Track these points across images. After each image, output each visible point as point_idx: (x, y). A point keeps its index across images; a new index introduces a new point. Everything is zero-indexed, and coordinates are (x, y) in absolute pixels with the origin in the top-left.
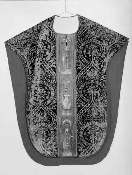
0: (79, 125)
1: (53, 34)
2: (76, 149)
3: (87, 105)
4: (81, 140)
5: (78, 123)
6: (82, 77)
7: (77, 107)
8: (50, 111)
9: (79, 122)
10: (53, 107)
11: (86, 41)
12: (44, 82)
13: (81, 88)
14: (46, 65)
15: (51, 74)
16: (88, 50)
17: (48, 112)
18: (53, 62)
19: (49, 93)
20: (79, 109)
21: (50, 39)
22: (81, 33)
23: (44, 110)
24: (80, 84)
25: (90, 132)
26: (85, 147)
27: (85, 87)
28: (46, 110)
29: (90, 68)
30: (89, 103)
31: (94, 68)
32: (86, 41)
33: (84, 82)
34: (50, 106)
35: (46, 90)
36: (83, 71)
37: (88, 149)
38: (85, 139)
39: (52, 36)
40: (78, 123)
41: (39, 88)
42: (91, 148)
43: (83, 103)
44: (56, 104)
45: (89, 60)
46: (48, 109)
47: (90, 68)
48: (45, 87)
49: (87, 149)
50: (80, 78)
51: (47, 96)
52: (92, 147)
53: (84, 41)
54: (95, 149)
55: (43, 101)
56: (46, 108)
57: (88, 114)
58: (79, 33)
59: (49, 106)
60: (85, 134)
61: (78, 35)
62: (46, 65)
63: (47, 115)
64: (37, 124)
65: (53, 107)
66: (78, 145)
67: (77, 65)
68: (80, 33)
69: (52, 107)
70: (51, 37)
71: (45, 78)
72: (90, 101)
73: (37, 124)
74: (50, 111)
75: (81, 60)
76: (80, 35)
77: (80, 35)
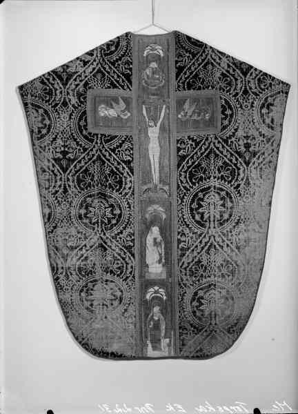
0: (182, 187)
2: (175, 244)
3: (201, 149)
4: (185, 222)
7: (176, 68)
8: (118, 76)
9: (182, 182)
10: (127, 241)
11: (199, 281)
13: (188, 199)
14: (110, 68)
16: (202, 301)
21: (121, 193)
22: (189, 167)
24: (185, 187)
27: (196, 195)
28: (108, 73)
29: (207, 152)
30: (204, 144)
32: (199, 281)
33: (194, 184)
37: (201, 242)
38: (194, 218)
41: (96, 201)
43: (188, 57)
44: (132, 149)
45: (203, 225)
47: (207, 152)
49: (199, 241)
51: (115, 300)
53: (194, 184)
54: (215, 241)
55: (105, 140)
56: (110, 155)
57: (200, 79)
58: (181, 78)
59: (118, 239)
61: (179, 82)
62: (110, 68)
65: (126, 69)
66: (180, 328)
67: (181, 331)
68: (186, 168)
71: (108, 181)
74: (118, 75)
75: (184, 48)
77: (185, 172)
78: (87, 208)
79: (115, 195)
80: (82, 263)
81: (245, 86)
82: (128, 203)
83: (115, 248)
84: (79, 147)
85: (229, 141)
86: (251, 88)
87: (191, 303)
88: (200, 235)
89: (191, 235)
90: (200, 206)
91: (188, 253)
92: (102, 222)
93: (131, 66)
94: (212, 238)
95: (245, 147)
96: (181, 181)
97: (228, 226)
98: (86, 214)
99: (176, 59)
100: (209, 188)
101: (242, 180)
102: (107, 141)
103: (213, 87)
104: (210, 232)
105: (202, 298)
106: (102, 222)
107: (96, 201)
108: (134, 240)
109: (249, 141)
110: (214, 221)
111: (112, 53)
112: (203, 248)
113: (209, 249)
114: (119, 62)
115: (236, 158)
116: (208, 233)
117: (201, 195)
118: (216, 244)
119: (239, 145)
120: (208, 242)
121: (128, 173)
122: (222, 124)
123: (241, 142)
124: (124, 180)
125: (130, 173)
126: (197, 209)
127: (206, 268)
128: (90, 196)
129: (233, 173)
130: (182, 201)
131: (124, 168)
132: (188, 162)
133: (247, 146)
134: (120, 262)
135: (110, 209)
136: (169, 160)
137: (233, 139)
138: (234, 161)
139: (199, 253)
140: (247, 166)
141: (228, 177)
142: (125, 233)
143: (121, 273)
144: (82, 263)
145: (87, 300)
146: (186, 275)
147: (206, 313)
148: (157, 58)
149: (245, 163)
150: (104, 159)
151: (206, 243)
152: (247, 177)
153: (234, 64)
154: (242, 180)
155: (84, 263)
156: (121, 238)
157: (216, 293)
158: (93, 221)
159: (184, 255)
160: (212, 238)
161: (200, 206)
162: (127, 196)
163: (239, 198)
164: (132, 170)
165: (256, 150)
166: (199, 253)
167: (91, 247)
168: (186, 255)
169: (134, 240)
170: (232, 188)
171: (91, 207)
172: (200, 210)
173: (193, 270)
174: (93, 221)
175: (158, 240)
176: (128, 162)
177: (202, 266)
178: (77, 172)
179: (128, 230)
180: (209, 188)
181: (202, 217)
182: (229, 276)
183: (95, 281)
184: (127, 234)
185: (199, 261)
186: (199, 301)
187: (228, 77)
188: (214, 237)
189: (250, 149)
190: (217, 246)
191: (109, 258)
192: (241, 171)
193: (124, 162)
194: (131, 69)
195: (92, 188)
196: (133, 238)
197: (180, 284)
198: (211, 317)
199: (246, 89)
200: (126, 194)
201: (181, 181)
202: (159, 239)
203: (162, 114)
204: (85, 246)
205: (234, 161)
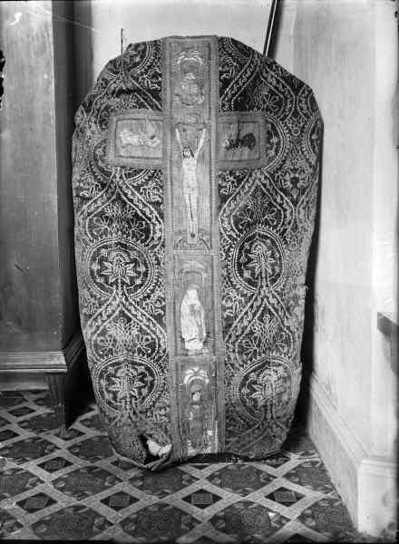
0: (226, 237)
4: (232, 282)
5: (222, 231)
7: (220, 80)
10: (156, 308)
11: (251, 360)
12: (136, 354)
15: (152, 331)
19: (150, 378)
20: (225, 83)
23: (127, 201)
24: (230, 236)
25: (261, 384)
26: (235, 180)
28: (136, 316)
30: (249, 66)
31: (270, 312)
32: (251, 360)
34: (147, 304)
35: (135, 261)
36: (237, 82)
37: (252, 307)
40: (222, 231)
41: (114, 254)
44: (161, 187)
45: (254, 285)
48: (131, 253)
51: (144, 387)
52: (262, 300)
56: (133, 194)
59: (141, 191)
60: (247, 274)
61: (224, 99)
62: (136, 309)
63: (141, 330)
64: (112, 354)
65: (152, 83)
72: (252, 62)
73: (112, 354)
76: (233, 343)
77: (233, 343)
78: (100, 263)
79: (140, 246)
80: (99, 339)
81: (296, 107)
82: (157, 259)
83: (140, 316)
84: (96, 183)
85: (276, 175)
86: (301, 109)
87: (240, 390)
88: (251, 298)
89: (239, 297)
90: (250, 260)
91: (235, 323)
92: (123, 283)
93: (160, 79)
94: (265, 300)
95: (292, 182)
96: (224, 228)
97: (281, 281)
98: (99, 272)
99: (221, 69)
100: (254, 236)
101: (289, 223)
102: (129, 176)
103: (259, 109)
104: (262, 292)
105: (255, 383)
106: (123, 283)
107: (114, 254)
108: (164, 307)
109: (297, 175)
110: (266, 278)
111: (136, 65)
112: (254, 315)
113: (262, 315)
114: (145, 76)
115: (281, 196)
116: (260, 293)
117: (247, 246)
118: (270, 307)
119: (285, 181)
120: (260, 306)
121: (157, 219)
122: (267, 155)
123: (287, 177)
124: (152, 228)
125: (160, 219)
126: (245, 264)
127: (260, 341)
128: (105, 247)
129: (278, 216)
130: (228, 256)
131: (151, 212)
132: (229, 205)
133: (294, 181)
134: (150, 338)
135: (132, 265)
136: (211, 200)
137: (280, 173)
138: (279, 200)
139: (250, 322)
140: (295, 206)
141: (273, 221)
142: (154, 297)
143: (153, 351)
144: (99, 339)
145: (109, 392)
146: (234, 351)
147: (261, 404)
148: (193, 68)
149: (293, 203)
150: (124, 198)
151: (259, 307)
152: (295, 219)
153: (283, 78)
154: (289, 223)
155: (101, 338)
156: (147, 304)
157: (272, 373)
158: (111, 281)
159: (230, 325)
160: (265, 300)
161: (250, 260)
162: (156, 250)
163: (284, 246)
164: (162, 215)
165: (305, 186)
166: (250, 322)
167: (109, 317)
168: (233, 326)
169: (164, 307)
170: (278, 235)
171: (107, 261)
172: (250, 265)
173: (244, 345)
174: (111, 281)
175: (196, 308)
176: (158, 204)
177: (256, 338)
178: (233, 95)
179: (158, 293)
180: (254, 236)
181: (253, 275)
182: (283, 347)
183: (118, 364)
184: (155, 298)
185: (252, 333)
186: (250, 386)
187: (277, 95)
188: (268, 298)
189: (298, 185)
190: (272, 310)
191: (135, 332)
192: (288, 213)
193: (151, 203)
194: (159, 83)
195: (109, 236)
196: (163, 303)
197: (226, 364)
198: (266, 410)
199: (296, 110)
200: (154, 246)
201: (224, 228)
202: (198, 304)
203: (202, 141)
204: (101, 314)
205: (279, 200)
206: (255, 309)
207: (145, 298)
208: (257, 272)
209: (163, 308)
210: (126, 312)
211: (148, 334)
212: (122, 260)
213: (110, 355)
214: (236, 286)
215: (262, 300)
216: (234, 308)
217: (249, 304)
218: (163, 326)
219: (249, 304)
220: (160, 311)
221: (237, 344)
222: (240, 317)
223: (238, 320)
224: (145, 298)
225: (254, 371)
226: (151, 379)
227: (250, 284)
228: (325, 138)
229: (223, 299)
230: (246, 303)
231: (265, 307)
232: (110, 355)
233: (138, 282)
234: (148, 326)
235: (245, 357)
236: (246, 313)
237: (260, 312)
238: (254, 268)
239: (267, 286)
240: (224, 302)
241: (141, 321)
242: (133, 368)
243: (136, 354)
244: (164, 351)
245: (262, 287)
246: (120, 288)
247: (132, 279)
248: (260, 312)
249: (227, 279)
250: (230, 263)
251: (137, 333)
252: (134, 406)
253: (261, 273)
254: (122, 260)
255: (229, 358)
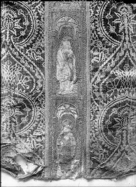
1: (37, 84)
4: (99, 35)
6: (103, 82)
10: (37, 143)
11: (113, 97)
12: (17, 89)
17: (23, 64)
18: (35, 50)
19: (26, 23)
31: (130, 63)
35: (21, 17)
39: (35, 89)
42: (119, 153)
46: (25, 59)
50: (98, 84)
51: (24, 116)
52: (125, 52)
59: (27, 52)
69: (33, 54)
70: (32, 90)
82: (38, 14)
88: (115, 49)
94: (127, 52)
113: (124, 64)
118: (130, 59)
130: (95, 12)
134: (29, 78)
135: (19, 20)
146: (99, 91)
151: (121, 58)
156: (30, 52)
160: (127, 52)
161: (115, 17)
162: (37, 7)
172: (116, 22)
179: (38, 43)
181: (117, 29)
184: (36, 47)
188: (129, 52)
197: (92, 101)
198: (122, 137)
206: (117, 59)
207: (28, 47)
208: (121, 29)
209: (43, 55)
210: (12, 57)
211: (27, 74)
212: (11, 16)
213: (115, 97)
214: (102, 38)
215: (125, 52)
216: (100, 56)
217: (113, 55)
218: (42, 69)
219: (113, 55)
220: (40, 57)
221: (101, 85)
222: (105, 63)
223: (103, 65)
224: (28, 47)
225: (115, 106)
226: (29, 110)
227: (113, 38)
228: (100, 180)
229: (91, 49)
230: (111, 53)
231: (126, 59)
232: (115, 97)
233: (23, 33)
234: (28, 69)
235: (108, 95)
236: (110, 61)
237: (122, 61)
238: (118, 24)
239: (129, 42)
240: (92, 51)
241: (23, 64)
242: (14, 99)
243: (17, 89)
244: (41, 89)
245: (125, 41)
246: (8, 37)
247: (18, 31)
248: (122, 61)
249: (95, 32)
250: (96, 19)
251: (19, 73)
252: (14, 129)
253: (124, 30)
254: (11, 16)
255: (95, 97)
